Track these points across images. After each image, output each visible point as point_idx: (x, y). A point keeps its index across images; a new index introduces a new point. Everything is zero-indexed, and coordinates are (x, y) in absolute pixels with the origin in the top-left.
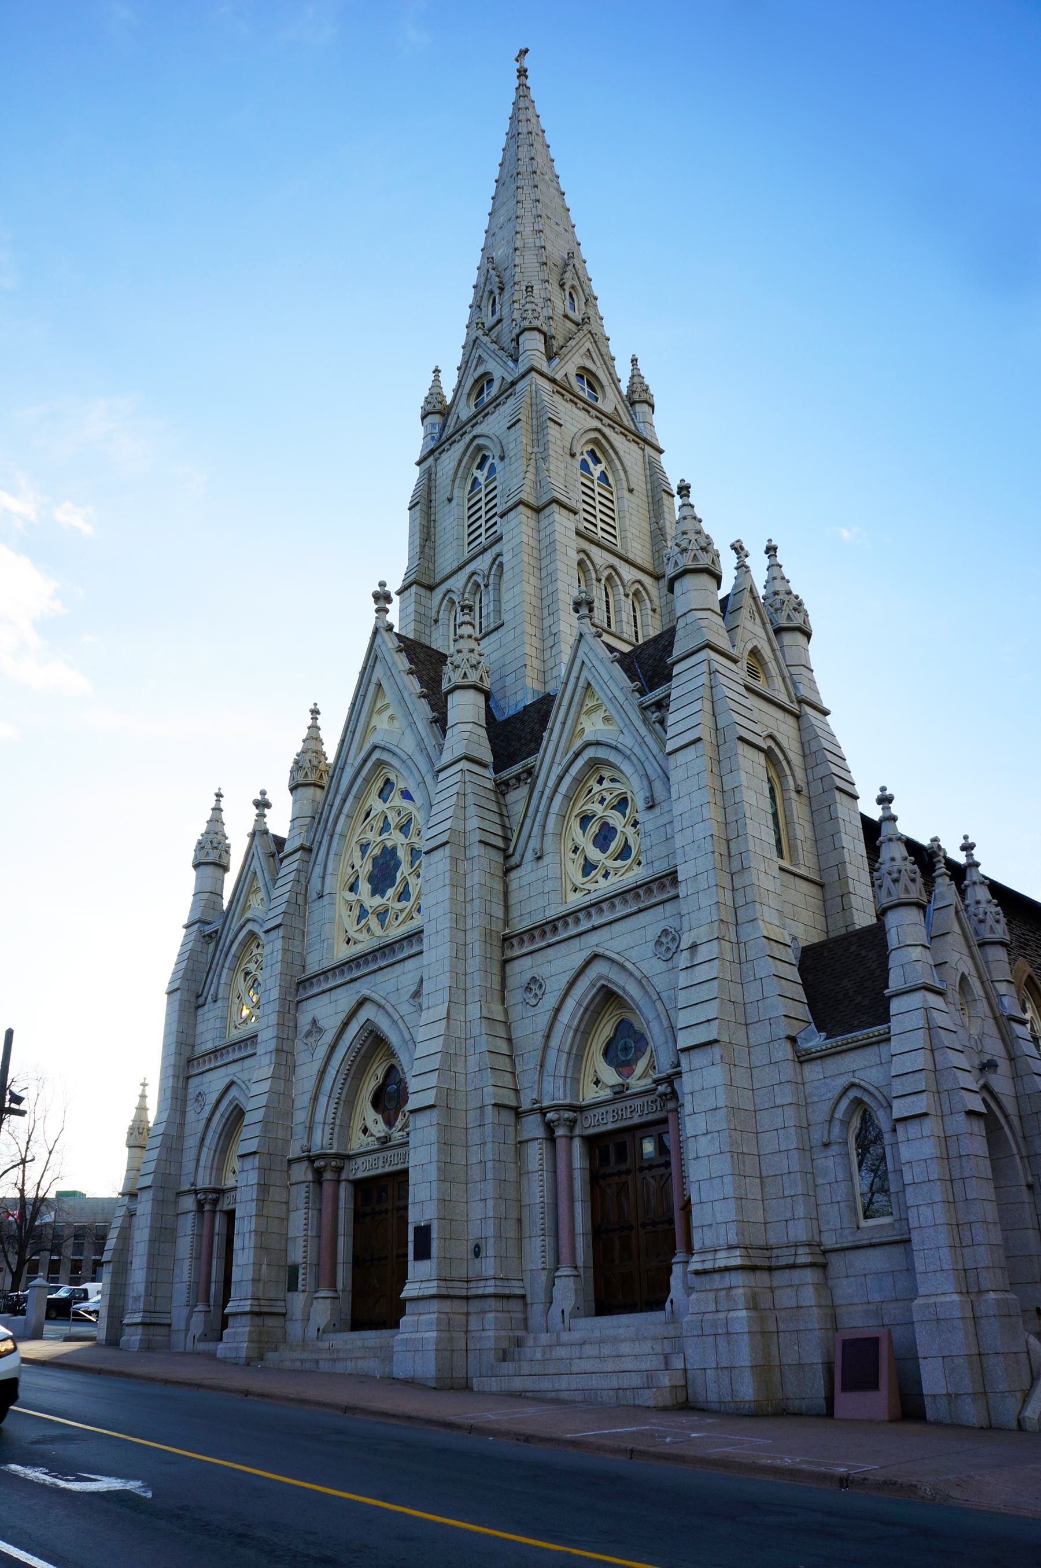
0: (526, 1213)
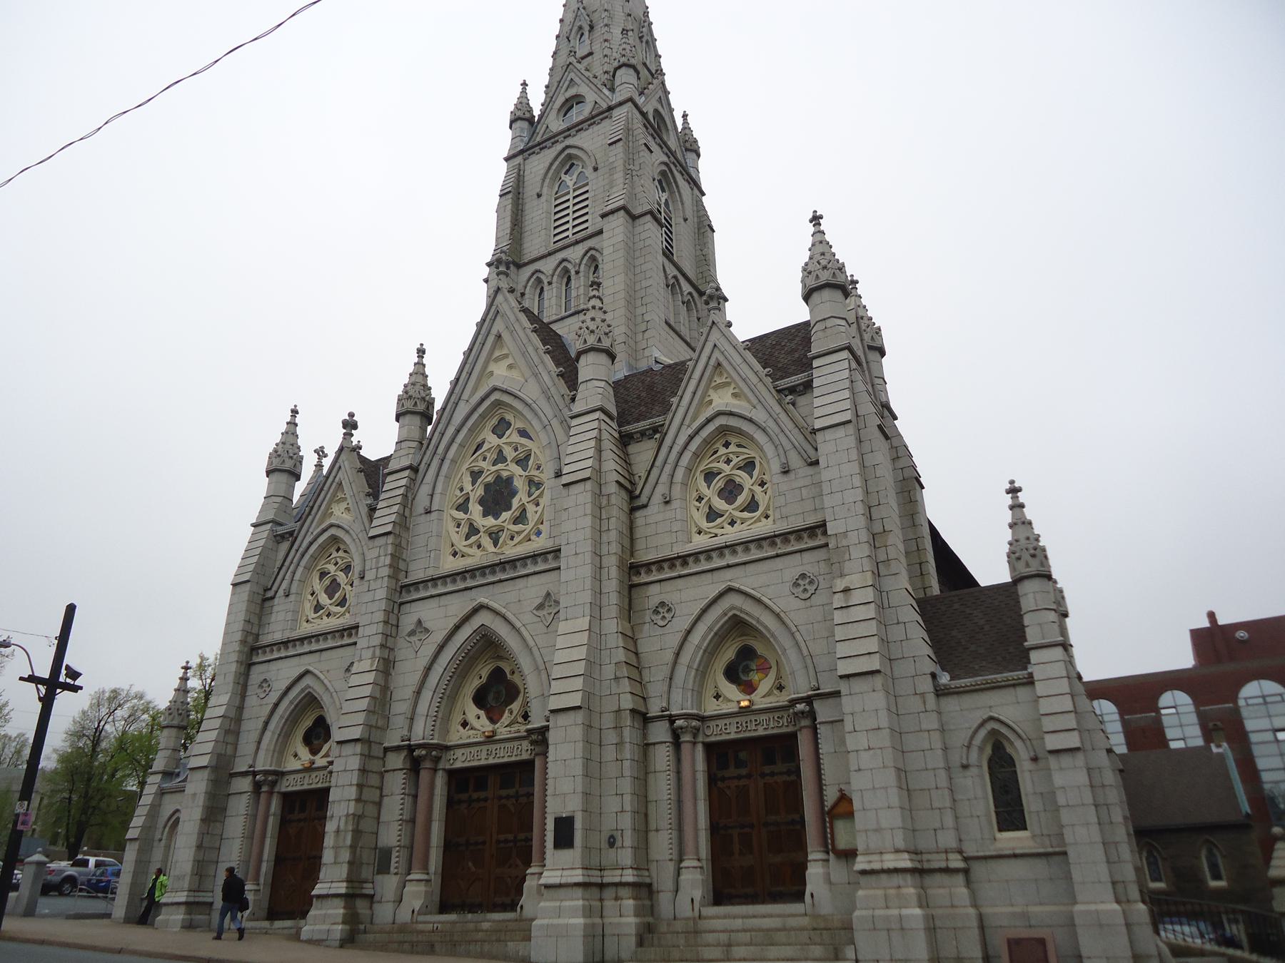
0: (652, 807)
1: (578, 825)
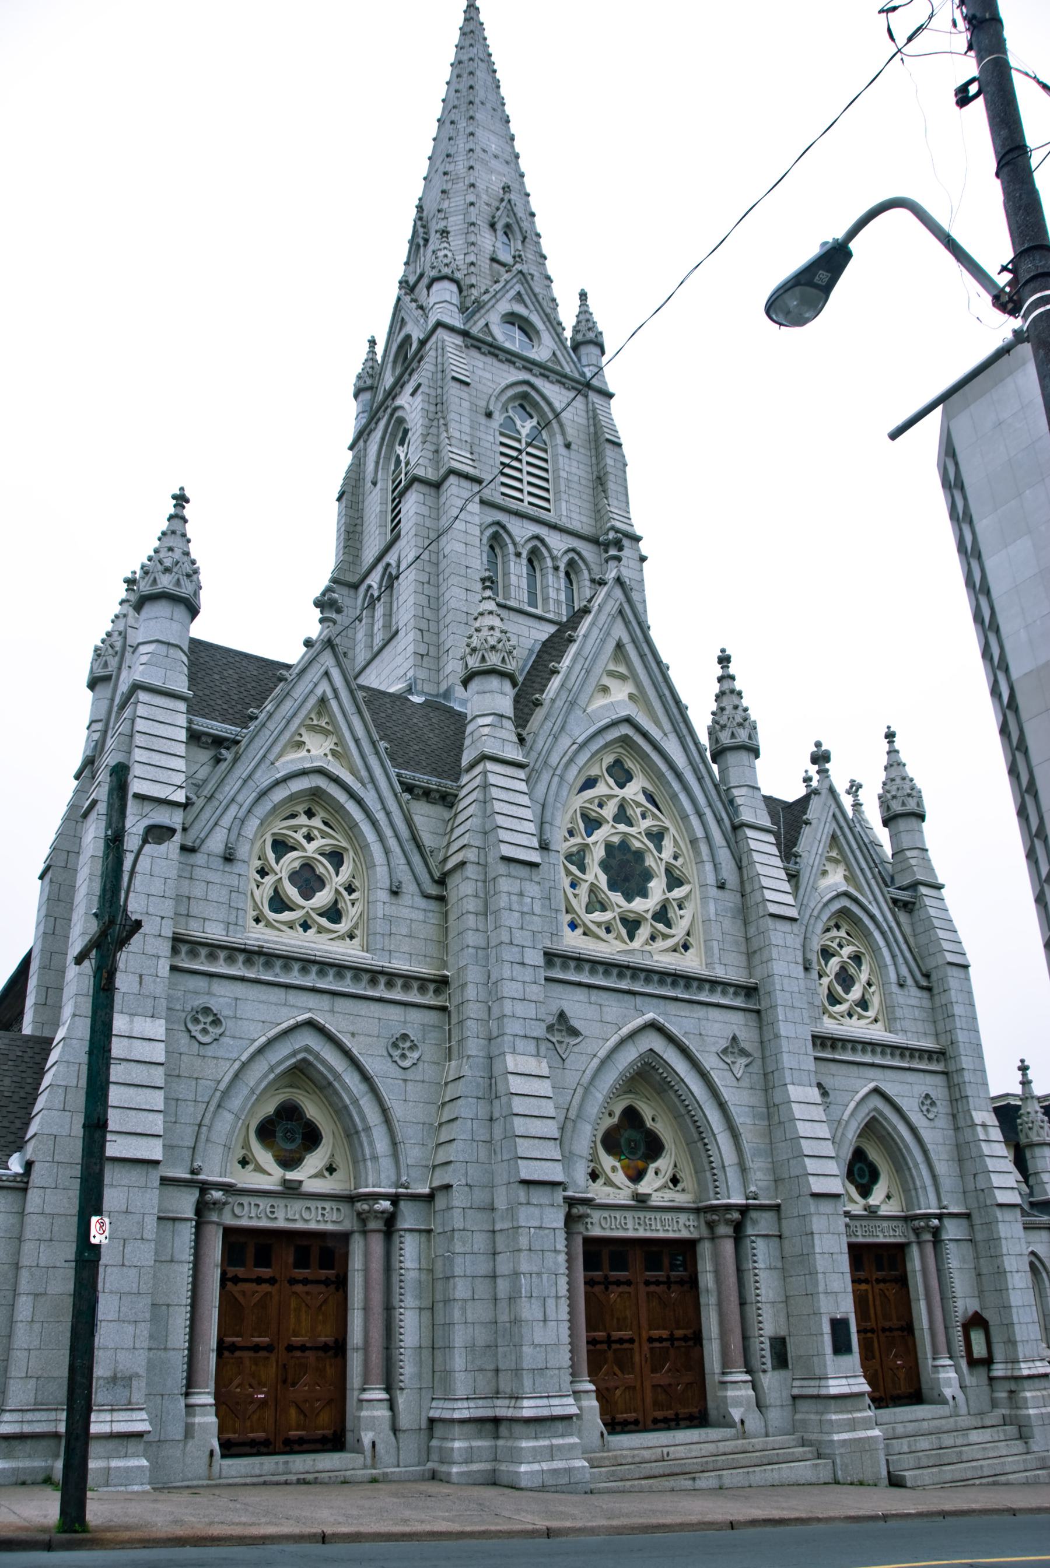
1: (828, 1348)
